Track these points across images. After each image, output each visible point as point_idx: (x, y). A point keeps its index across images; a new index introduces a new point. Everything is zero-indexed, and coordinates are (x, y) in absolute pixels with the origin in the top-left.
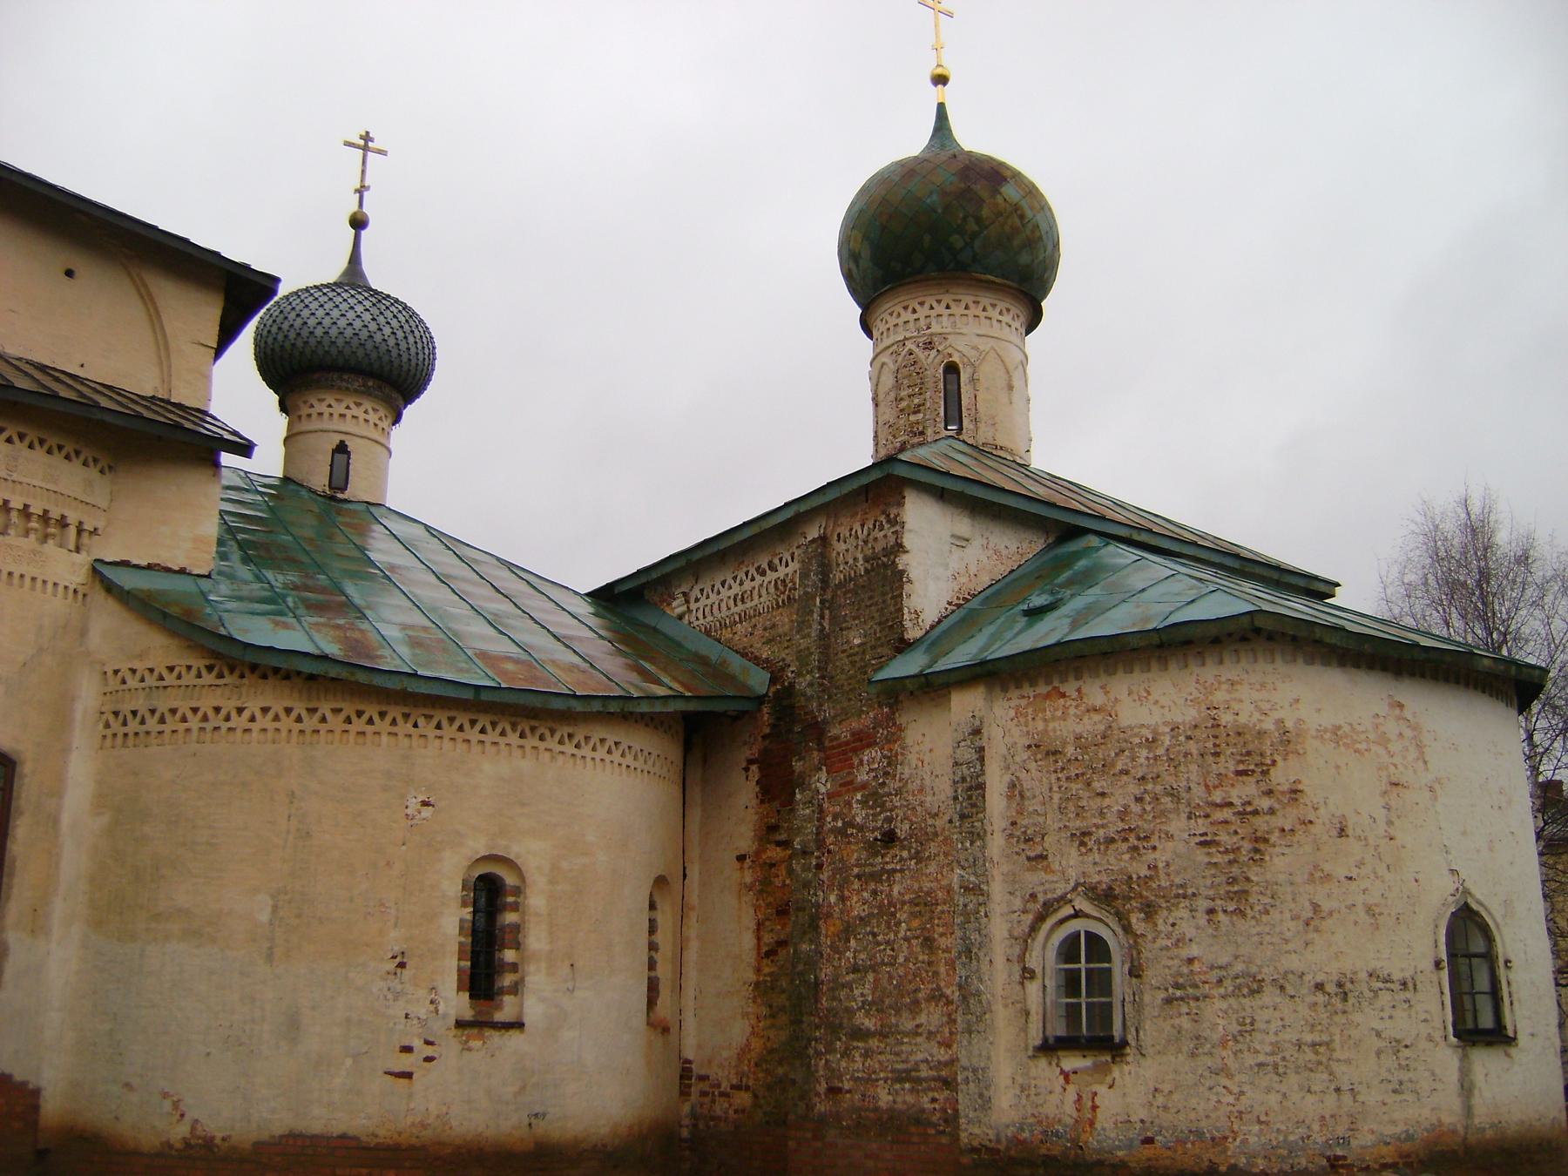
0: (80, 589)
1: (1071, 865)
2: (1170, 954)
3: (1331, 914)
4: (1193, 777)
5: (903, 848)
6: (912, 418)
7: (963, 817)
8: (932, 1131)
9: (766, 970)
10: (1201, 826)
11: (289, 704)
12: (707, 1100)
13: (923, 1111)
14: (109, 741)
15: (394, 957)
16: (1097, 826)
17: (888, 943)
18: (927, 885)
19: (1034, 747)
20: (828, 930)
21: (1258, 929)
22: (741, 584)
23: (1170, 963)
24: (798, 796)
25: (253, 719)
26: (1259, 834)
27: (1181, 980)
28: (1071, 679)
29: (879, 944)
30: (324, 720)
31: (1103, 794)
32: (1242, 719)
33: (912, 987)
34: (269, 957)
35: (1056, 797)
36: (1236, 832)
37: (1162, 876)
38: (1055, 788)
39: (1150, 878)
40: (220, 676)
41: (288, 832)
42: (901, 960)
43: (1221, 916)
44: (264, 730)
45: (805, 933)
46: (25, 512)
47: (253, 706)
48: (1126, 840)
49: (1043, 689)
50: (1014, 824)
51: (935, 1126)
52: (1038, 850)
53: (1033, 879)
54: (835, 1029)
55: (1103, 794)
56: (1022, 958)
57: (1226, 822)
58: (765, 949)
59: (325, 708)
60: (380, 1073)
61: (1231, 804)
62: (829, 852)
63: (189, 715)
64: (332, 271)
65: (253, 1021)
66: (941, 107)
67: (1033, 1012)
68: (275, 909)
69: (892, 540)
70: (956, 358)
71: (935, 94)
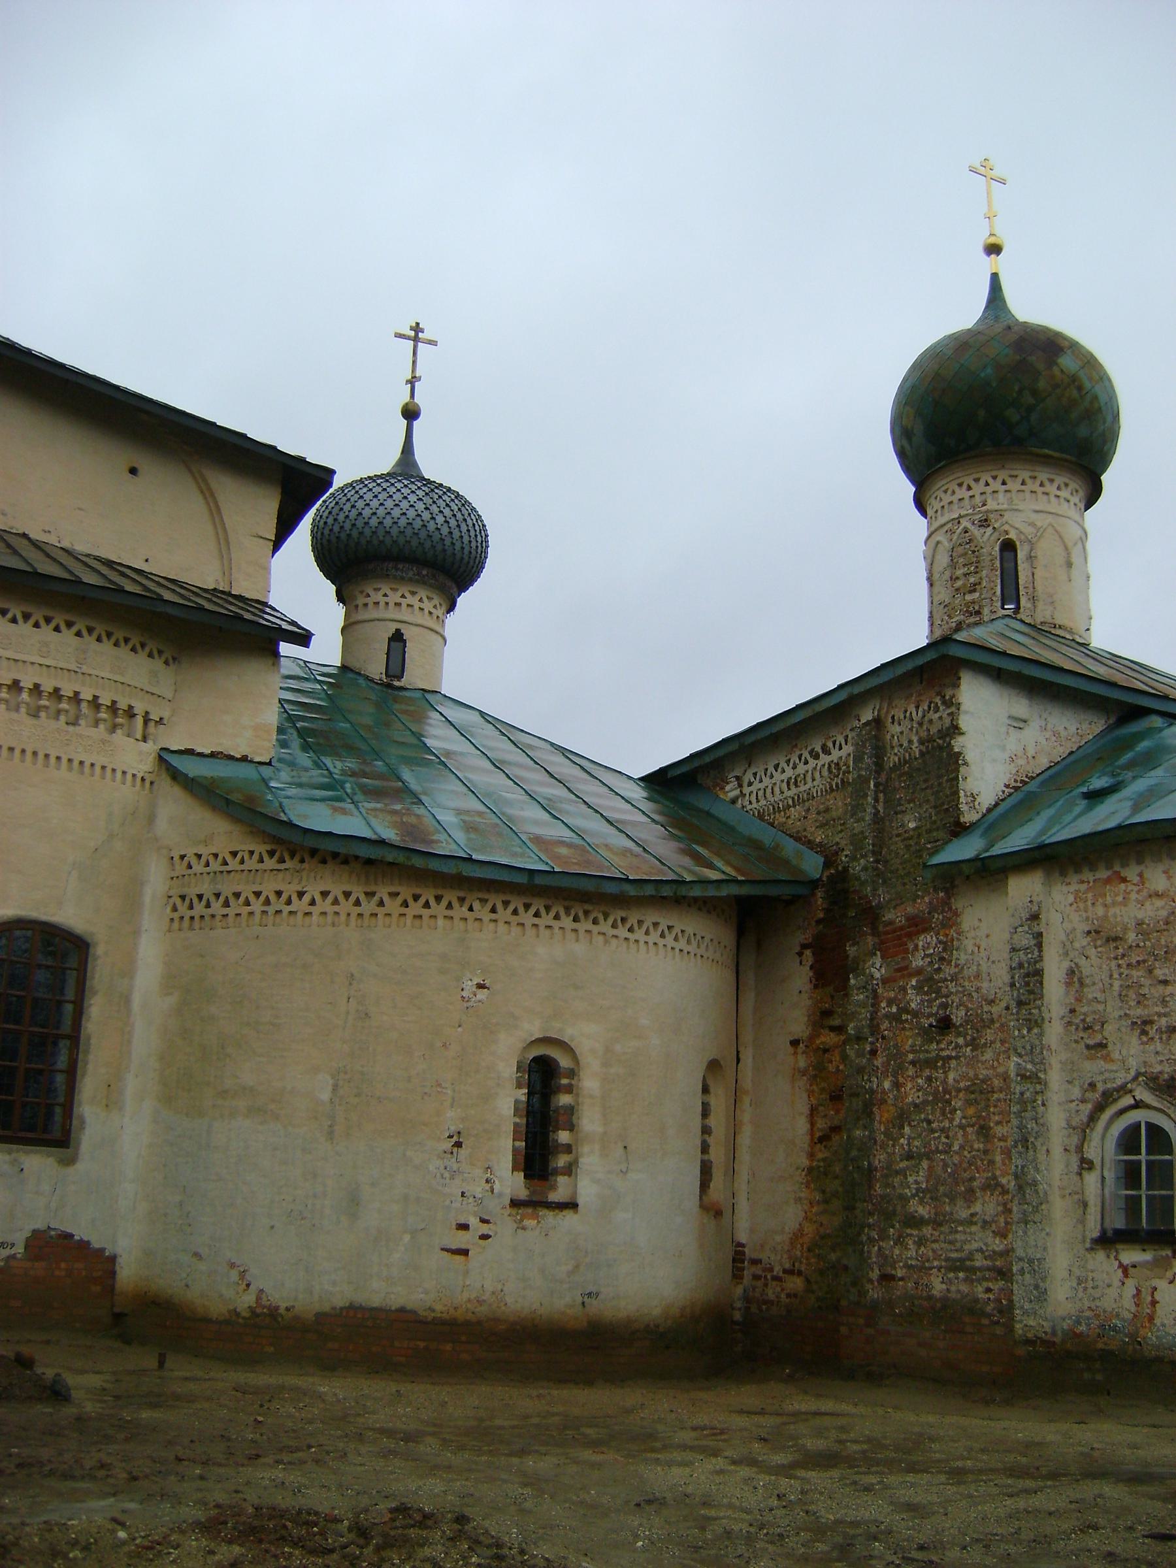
0: (147, 776)
1: (1131, 1055)
5: (959, 1034)
6: (968, 597)
7: (1020, 1003)
8: (985, 1321)
9: (820, 1156)
11: (348, 888)
12: (759, 1283)
13: (976, 1300)
14: (176, 925)
15: (451, 1137)
16: (1160, 1015)
17: (943, 1130)
18: (984, 1073)
20: (882, 1116)
22: (794, 768)
24: (852, 981)
25: (313, 903)
29: (933, 1131)
30: (381, 903)
31: (1165, 982)
33: (966, 1175)
34: (330, 1135)
38: (1116, 976)
40: (282, 860)
41: (348, 1013)
42: (956, 1147)
45: (858, 1119)
46: (95, 703)
47: (313, 891)
49: (1103, 874)
50: (1072, 1011)
51: (989, 1316)
52: (1098, 1038)
53: (1092, 1068)
54: (889, 1216)
55: (1165, 982)
56: (1080, 1149)
58: (818, 1134)
59: (383, 892)
60: (437, 1249)
62: (883, 1038)
63: (252, 898)
64: (386, 461)
65: (315, 1196)
66: (995, 278)
68: (335, 1088)
70: (1012, 535)
71: (988, 264)
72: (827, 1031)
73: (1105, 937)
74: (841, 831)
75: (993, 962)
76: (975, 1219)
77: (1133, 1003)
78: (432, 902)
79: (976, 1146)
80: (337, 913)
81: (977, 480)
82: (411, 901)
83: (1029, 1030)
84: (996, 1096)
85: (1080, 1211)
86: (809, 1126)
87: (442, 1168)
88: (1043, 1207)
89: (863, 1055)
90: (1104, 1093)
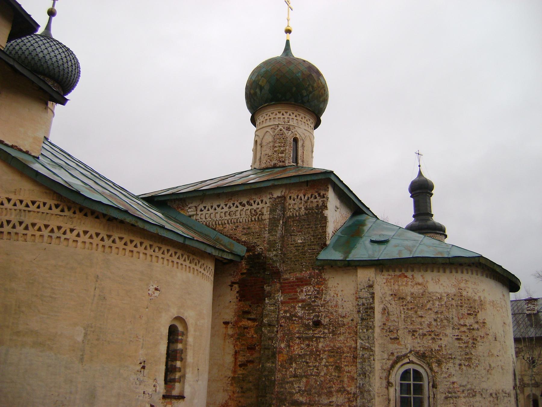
1: (408, 343)
2: (446, 380)
3: (494, 368)
4: (454, 313)
5: (325, 328)
6: (280, 155)
7: (362, 319)
9: (240, 372)
10: (457, 332)
11: (98, 231)
15: (141, 363)
16: (419, 329)
17: (315, 366)
18: (338, 345)
19: (394, 295)
20: (280, 358)
21: (475, 373)
22: (230, 207)
23: (447, 383)
24: (267, 301)
25: (78, 235)
26: (474, 337)
27: (450, 390)
28: (409, 271)
29: (309, 366)
30: (114, 242)
31: (422, 317)
32: (469, 294)
33: (328, 386)
34: (82, 360)
35: (403, 316)
36: (467, 336)
37: (444, 350)
38: (402, 312)
39: (439, 350)
40: (62, 211)
41: (94, 296)
42: (322, 374)
43: (463, 367)
44: (84, 242)
45: (269, 359)
47: (80, 229)
48: (430, 335)
49: (398, 273)
50: (384, 324)
52: (395, 336)
53: (392, 347)
55: (422, 317)
56: (387, 378)
57: (464, 332)
59: (116, 236)
61: (466, 325)
62: (281, 326)
63: (43, 228)
65: (71, 393)
66: (288, 42)
67: (392, 399)
68: (86, 335)
69: (320, 204)
70: (298, 136)
71: (285, 36)
72: (246, 320)
73: (399, 297)
74: (258, 238)
75: (345, 301)
76: (332, 404)
77: (409, 324)
78: (139, 245)
79: (334, 374)
80: (91, 243)
81: (286, 113)
82: (129, 243)
83: (367, 330)
84: (345, 355)
85: (387, 402)
86: (234, 359)
87: (136, 379)
88: (373, 400)
89: (273, 332)
90: (397, 357)
